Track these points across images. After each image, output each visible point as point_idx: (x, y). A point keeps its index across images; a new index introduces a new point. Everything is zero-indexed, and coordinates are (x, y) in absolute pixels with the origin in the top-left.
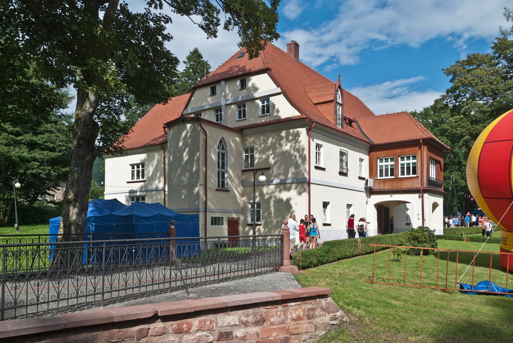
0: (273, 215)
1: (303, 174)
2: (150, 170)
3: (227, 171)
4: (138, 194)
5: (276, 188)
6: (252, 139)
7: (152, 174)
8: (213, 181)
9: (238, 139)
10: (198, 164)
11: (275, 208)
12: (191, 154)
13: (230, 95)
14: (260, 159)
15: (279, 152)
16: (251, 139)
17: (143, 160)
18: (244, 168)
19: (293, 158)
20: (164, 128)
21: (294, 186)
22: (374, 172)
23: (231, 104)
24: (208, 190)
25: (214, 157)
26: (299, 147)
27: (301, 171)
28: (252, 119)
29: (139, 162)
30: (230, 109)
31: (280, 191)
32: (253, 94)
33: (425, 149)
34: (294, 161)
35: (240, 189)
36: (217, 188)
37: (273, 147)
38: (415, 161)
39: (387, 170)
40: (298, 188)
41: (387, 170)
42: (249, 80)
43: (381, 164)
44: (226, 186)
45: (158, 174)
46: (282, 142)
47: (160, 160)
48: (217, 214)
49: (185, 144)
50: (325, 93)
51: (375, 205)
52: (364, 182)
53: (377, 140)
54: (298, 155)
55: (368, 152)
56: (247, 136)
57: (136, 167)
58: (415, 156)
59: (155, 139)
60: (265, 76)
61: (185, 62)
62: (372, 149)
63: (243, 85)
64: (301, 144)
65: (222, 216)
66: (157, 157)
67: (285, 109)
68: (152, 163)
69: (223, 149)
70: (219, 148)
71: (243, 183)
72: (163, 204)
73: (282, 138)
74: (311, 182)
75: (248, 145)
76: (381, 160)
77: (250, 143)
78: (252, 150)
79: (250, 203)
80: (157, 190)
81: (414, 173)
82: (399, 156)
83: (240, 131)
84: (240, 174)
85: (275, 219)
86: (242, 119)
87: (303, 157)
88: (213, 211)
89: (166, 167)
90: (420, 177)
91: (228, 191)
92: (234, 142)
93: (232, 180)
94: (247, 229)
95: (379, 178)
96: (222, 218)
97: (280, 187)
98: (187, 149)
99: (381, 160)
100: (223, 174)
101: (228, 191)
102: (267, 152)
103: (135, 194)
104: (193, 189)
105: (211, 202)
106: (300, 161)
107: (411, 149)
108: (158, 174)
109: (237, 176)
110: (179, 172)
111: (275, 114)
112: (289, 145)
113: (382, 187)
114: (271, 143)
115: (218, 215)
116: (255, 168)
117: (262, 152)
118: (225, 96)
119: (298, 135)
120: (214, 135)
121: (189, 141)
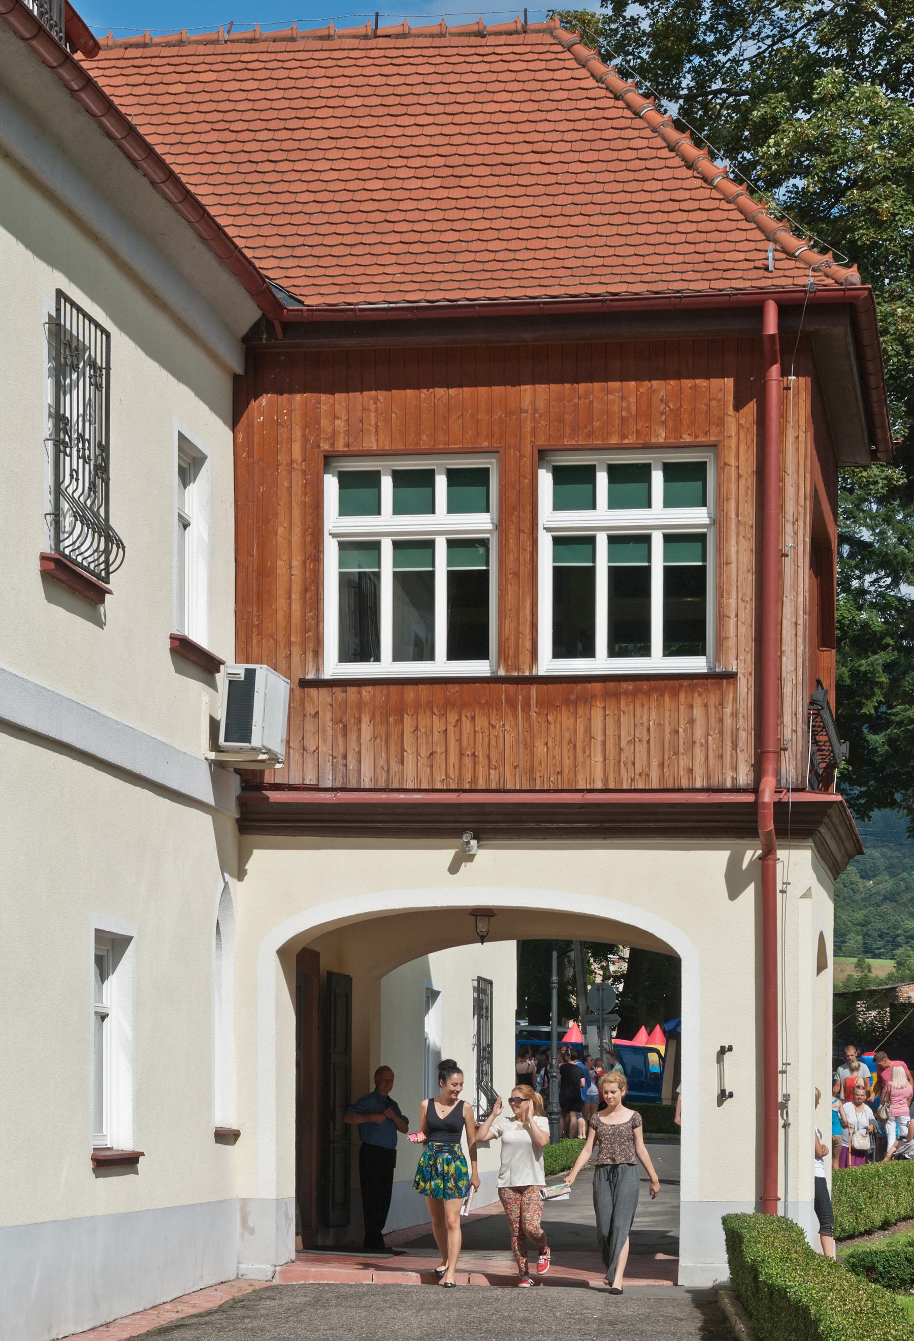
22: (286, 604)
33: (792, 396)
38: (694, 517)
39: (630, 585)
41: (630, 585)
43: (360, 525)
52: (210, 701)
53: (312, 285)
55: (224, 388)
58: (697, 471)
62: (280, 354)
76: (360, 491)
82: (542, 455)
90: (745, 686)
95: (333, 666)
113: (369, 768)
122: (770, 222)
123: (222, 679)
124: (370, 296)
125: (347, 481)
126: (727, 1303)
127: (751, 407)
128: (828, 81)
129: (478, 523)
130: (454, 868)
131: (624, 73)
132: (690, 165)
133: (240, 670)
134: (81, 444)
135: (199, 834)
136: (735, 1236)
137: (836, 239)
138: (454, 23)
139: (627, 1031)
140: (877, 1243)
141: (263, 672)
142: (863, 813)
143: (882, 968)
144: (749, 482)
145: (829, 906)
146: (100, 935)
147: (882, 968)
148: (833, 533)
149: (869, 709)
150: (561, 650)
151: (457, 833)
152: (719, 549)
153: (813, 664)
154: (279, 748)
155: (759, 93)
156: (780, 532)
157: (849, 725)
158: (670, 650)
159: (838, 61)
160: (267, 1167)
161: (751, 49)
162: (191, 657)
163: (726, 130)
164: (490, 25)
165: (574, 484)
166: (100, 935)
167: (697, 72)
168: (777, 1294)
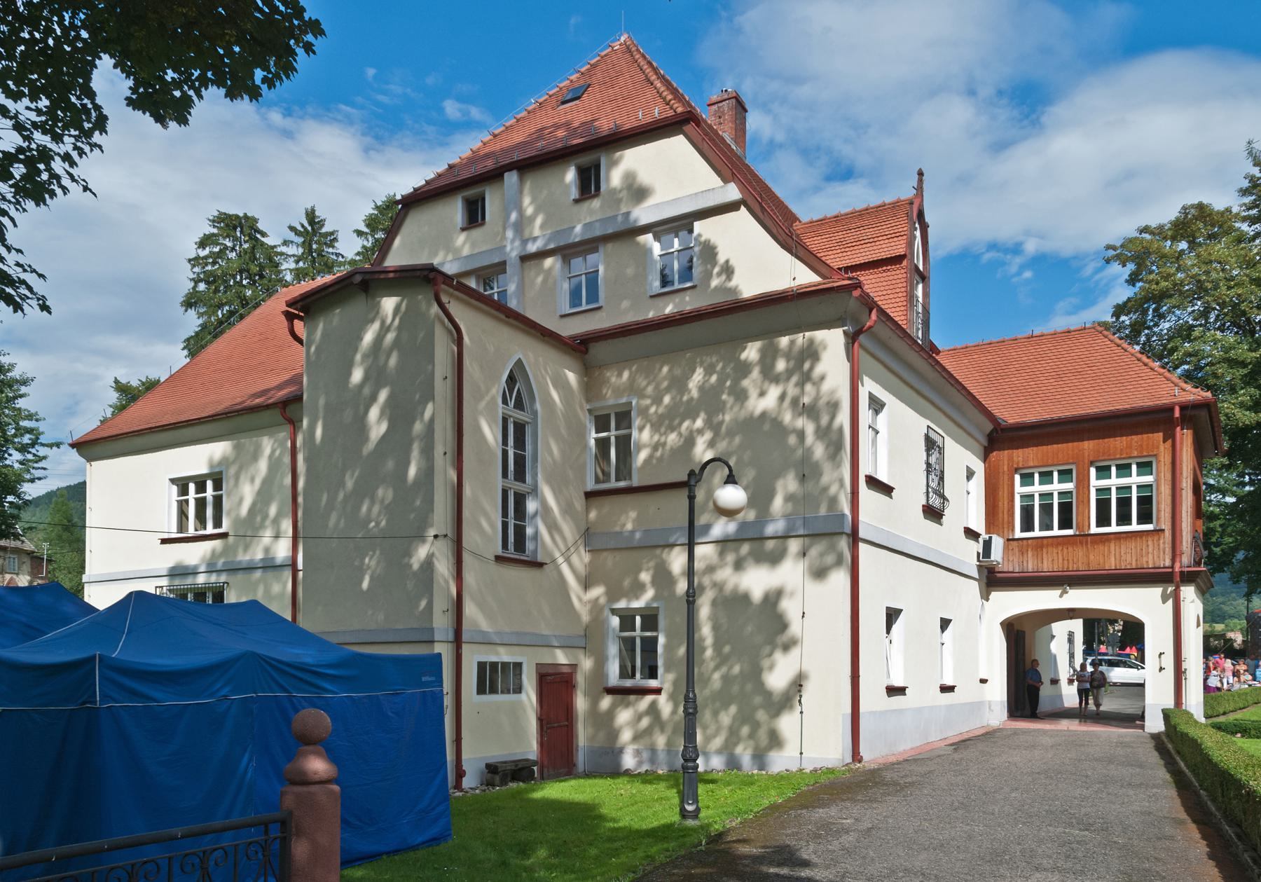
0: (709, 653)
1: (834, 501)
2: (243, 495)
3: (535, 491)
4: (201, 579)
5: (722, 554)
6: (626, 375)
7: (252, 511)
8: (485, 528)
9: (572, 377)
10: (428, 452)
11: (715, 628)
12: (400, 415)
13: (539, 221)
14: (655, 448)
15: (735, 420)
16: (620, 375)
17: (220, 463)
18: (591, 485)
19: (792, 440)
20: (290, 317)
21: (794, 546)
23: (542, 255)
24: (466, 557)
25: (490, 433)
26: (817, 398)
27: (826, 489)
28: (625, 304)
29: (203, 470)
30: (541, 270)
31: (739, 566)
32: (628, 214)
33: (1185, 438)
34: (793, 450)
35: (582, 559)
36: (499, 551)
37: (710, 402)
39: (1124, 503)
40: (814, 552)
41: (1124, 503)
42: (615, 163)
44: (530, 546)
45: (273, 510)
46: (746, 383)
47: (279, 459)
48: (501, 649)
49: (376, 377)
50: (870, 232)
52: (979, 547)
53: (1010, 415)
54: (810, 429)
55: (980, 450)
56: (603, 366)
57: (192, 487)
58: (1149, 464)
59: (263, 393)
60: (678, 147)
61: (359, 233)
62: (999, 439)
63: (589, 183)
64: (826, 387)
65: (518, 660)
66: (267, 451)
67: (756, 263)
68: (252, 469)
69: (519, 405)
70: (505, 402)
71: (588, 536)
72: (290, 619)
73: (745, 369)
74: (862, 534)
75: (611, 402)
76: (1027, 479)
77: (618, 392)
78: (624, 418)
79: (614, 612)
80: (269, 566)
81: (1145, 517)
82: (1092, 463)
83: (579, 348)
84: (579, 503)
85: (717, 668)
87: (834, 436)
88: (487, 642)
89: (301, 484)
90: (1168, 534)
91: (540, 565)
92: (556, 384)
93: (553, 527)
94: (606, 702)
95: (1018, 534)
96: (518, 666)
97: (737, 550)
98: (383, 395)
99: (1027, 479)
100: (520, 500)
101: (540, 565)
102: (686, 424)
103: (189, 580)
104: (408, 554)
105: (482, 605)
106: (819, 451)
107: (1135, 438)
108: (273, 510)
109: (567, 510)
110: (350, 484)
111: (715, 282)
112: (774, 392)
113: (1030, 565)
114: (701, 388)
115: (504, 656)
116: (635, 482)
117: (665, 422)
118: (520, 227)
119: (812, 353)
120: (490, 347)
121: (393, 361)
122: (1177, 381)
123: (981, 540)
124: (1031, 418)
125: (1023, 476)
126: (1164, 738)
127: (1170, 441)
128: (1197, 332)
129: (1069, 486)
130: (1061, 596)
131: (1121, 339)
132: (1146, 365)
133: (987, 537)
134: (935, 471)
135: (974, 587)
136: (1166, 715)
137: (1201, 383)
138: (1059, 330)
139: (1122, 648)
140: (1222, 719)
141: (995, 537)
142: (1212, 574)
143: (1219, 627)
144: (1169, 466)
145: (1201, 606)
146: (942, 619)
147: (1219, 627)
148: (1202, 481)
149: (1214, 540)
150: (1099, 524)
151: (1062, 585)
152: (1158, 489)
153: (1194, 525)
154: (1000, 560)
155: (1169, 340)
156: (1181, 482)
157: (1207, 545)
158: (1139, 523)
159: (1201, 325)
160: (998, 691)
161: (1167, 325)
162: (971, 534)
163: (1162, 353)
164: (1072, 328)
165: (1103, 471)
166: (942, 619)
167: (1147, 335)
168: (1184, 736)
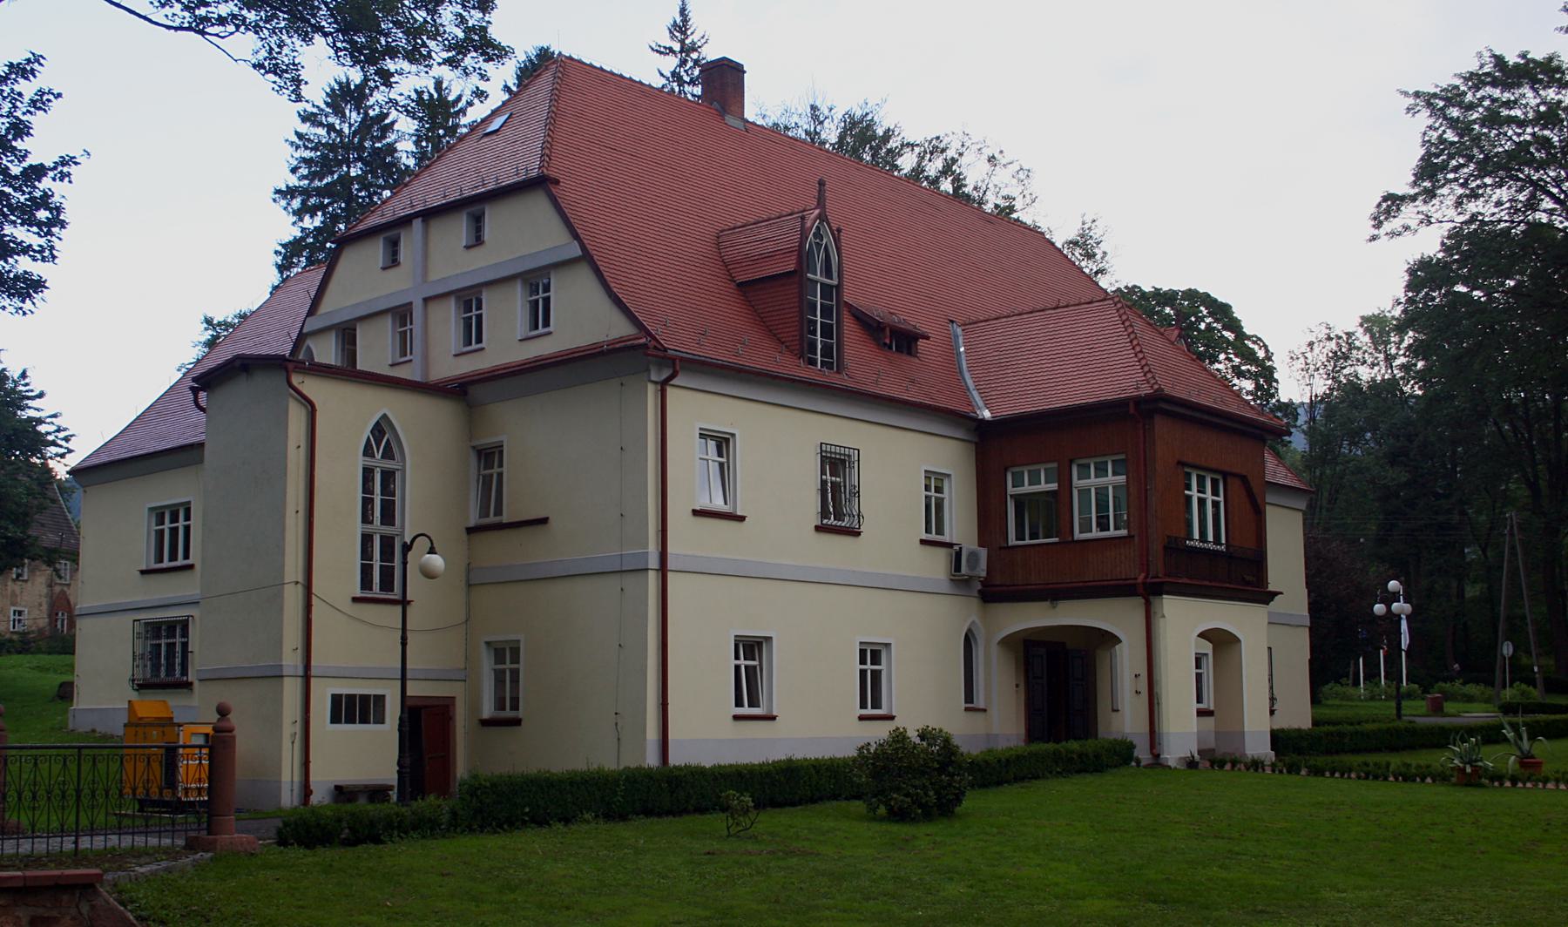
20: (195, 391)
24: (315, 600)
51: (453, 698)
69: (388, 454)
86: (541, 330)
